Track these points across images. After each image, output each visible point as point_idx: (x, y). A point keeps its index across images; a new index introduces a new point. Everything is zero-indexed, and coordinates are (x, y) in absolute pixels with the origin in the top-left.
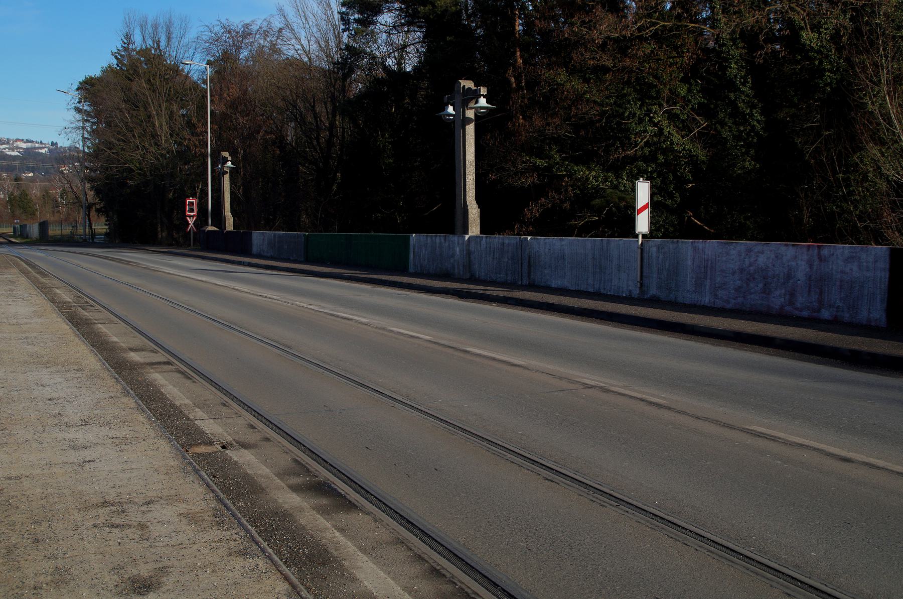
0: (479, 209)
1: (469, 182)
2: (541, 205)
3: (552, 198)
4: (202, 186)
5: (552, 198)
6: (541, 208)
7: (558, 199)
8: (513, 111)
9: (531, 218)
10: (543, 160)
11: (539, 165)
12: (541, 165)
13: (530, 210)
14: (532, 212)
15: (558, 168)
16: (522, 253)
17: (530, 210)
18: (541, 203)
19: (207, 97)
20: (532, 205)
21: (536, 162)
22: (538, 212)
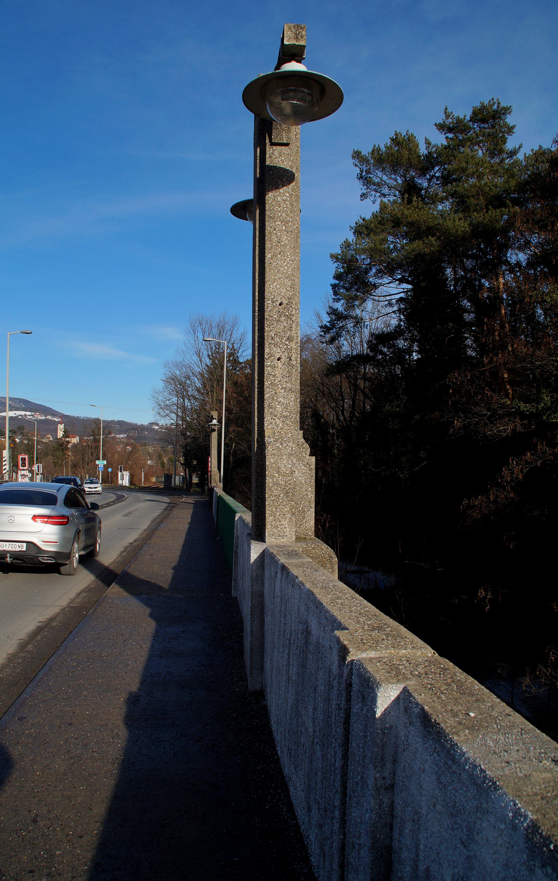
0: (313, 459)
1: (274, 367)
2: (527, 463)
3: (542, 453)
4: (229, 460)
5: (542, 453)
6: (526, 468)
7: (550, 455)
8: (490, 344)
9: (511, 481)
10: (529, 403)
11: (524, 411)
12: (527, 411)
13: (510, 470)
14: (513, 473)
15: (550, 415)
16: (343, 803)
17: (509, 470)
18: (526, 460)
19: (223, 377)
20: (513, 462)
21: (519, 407)
22: (522, 472)
